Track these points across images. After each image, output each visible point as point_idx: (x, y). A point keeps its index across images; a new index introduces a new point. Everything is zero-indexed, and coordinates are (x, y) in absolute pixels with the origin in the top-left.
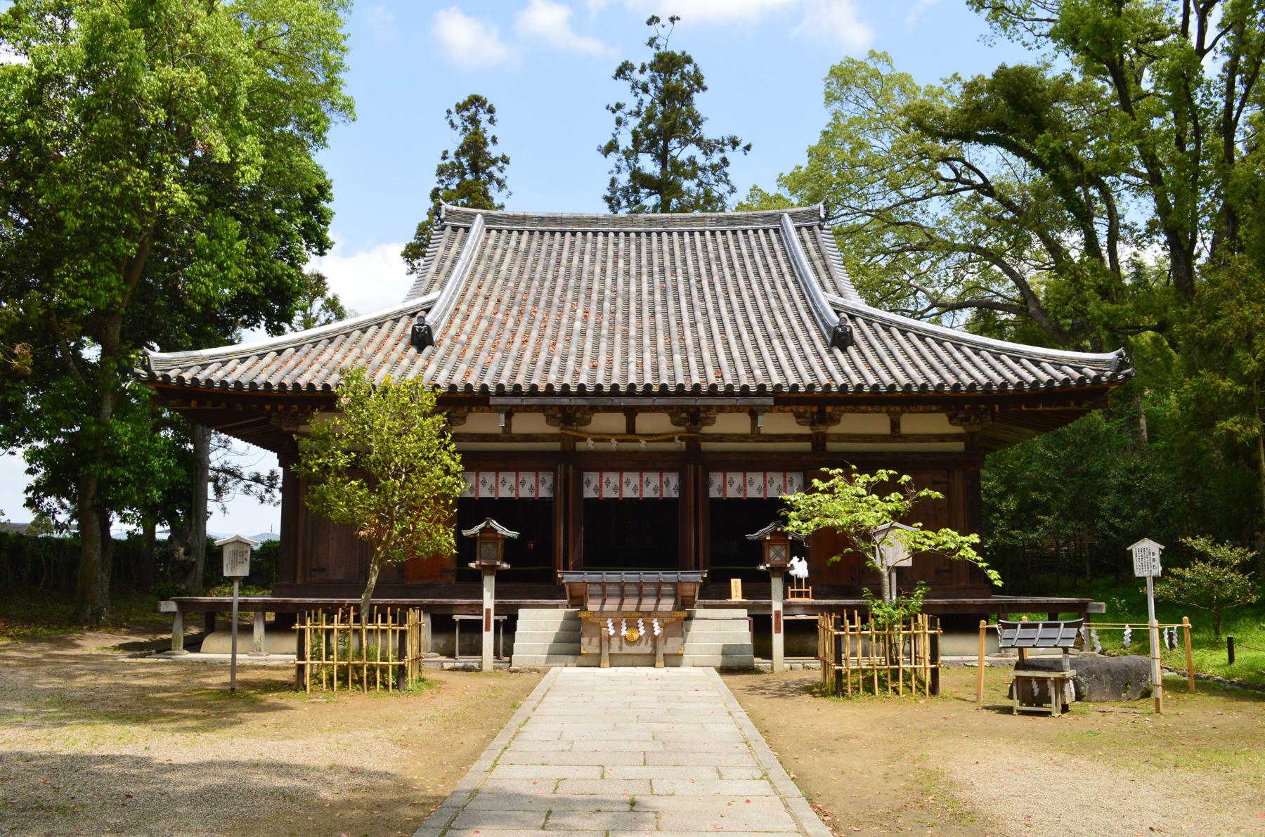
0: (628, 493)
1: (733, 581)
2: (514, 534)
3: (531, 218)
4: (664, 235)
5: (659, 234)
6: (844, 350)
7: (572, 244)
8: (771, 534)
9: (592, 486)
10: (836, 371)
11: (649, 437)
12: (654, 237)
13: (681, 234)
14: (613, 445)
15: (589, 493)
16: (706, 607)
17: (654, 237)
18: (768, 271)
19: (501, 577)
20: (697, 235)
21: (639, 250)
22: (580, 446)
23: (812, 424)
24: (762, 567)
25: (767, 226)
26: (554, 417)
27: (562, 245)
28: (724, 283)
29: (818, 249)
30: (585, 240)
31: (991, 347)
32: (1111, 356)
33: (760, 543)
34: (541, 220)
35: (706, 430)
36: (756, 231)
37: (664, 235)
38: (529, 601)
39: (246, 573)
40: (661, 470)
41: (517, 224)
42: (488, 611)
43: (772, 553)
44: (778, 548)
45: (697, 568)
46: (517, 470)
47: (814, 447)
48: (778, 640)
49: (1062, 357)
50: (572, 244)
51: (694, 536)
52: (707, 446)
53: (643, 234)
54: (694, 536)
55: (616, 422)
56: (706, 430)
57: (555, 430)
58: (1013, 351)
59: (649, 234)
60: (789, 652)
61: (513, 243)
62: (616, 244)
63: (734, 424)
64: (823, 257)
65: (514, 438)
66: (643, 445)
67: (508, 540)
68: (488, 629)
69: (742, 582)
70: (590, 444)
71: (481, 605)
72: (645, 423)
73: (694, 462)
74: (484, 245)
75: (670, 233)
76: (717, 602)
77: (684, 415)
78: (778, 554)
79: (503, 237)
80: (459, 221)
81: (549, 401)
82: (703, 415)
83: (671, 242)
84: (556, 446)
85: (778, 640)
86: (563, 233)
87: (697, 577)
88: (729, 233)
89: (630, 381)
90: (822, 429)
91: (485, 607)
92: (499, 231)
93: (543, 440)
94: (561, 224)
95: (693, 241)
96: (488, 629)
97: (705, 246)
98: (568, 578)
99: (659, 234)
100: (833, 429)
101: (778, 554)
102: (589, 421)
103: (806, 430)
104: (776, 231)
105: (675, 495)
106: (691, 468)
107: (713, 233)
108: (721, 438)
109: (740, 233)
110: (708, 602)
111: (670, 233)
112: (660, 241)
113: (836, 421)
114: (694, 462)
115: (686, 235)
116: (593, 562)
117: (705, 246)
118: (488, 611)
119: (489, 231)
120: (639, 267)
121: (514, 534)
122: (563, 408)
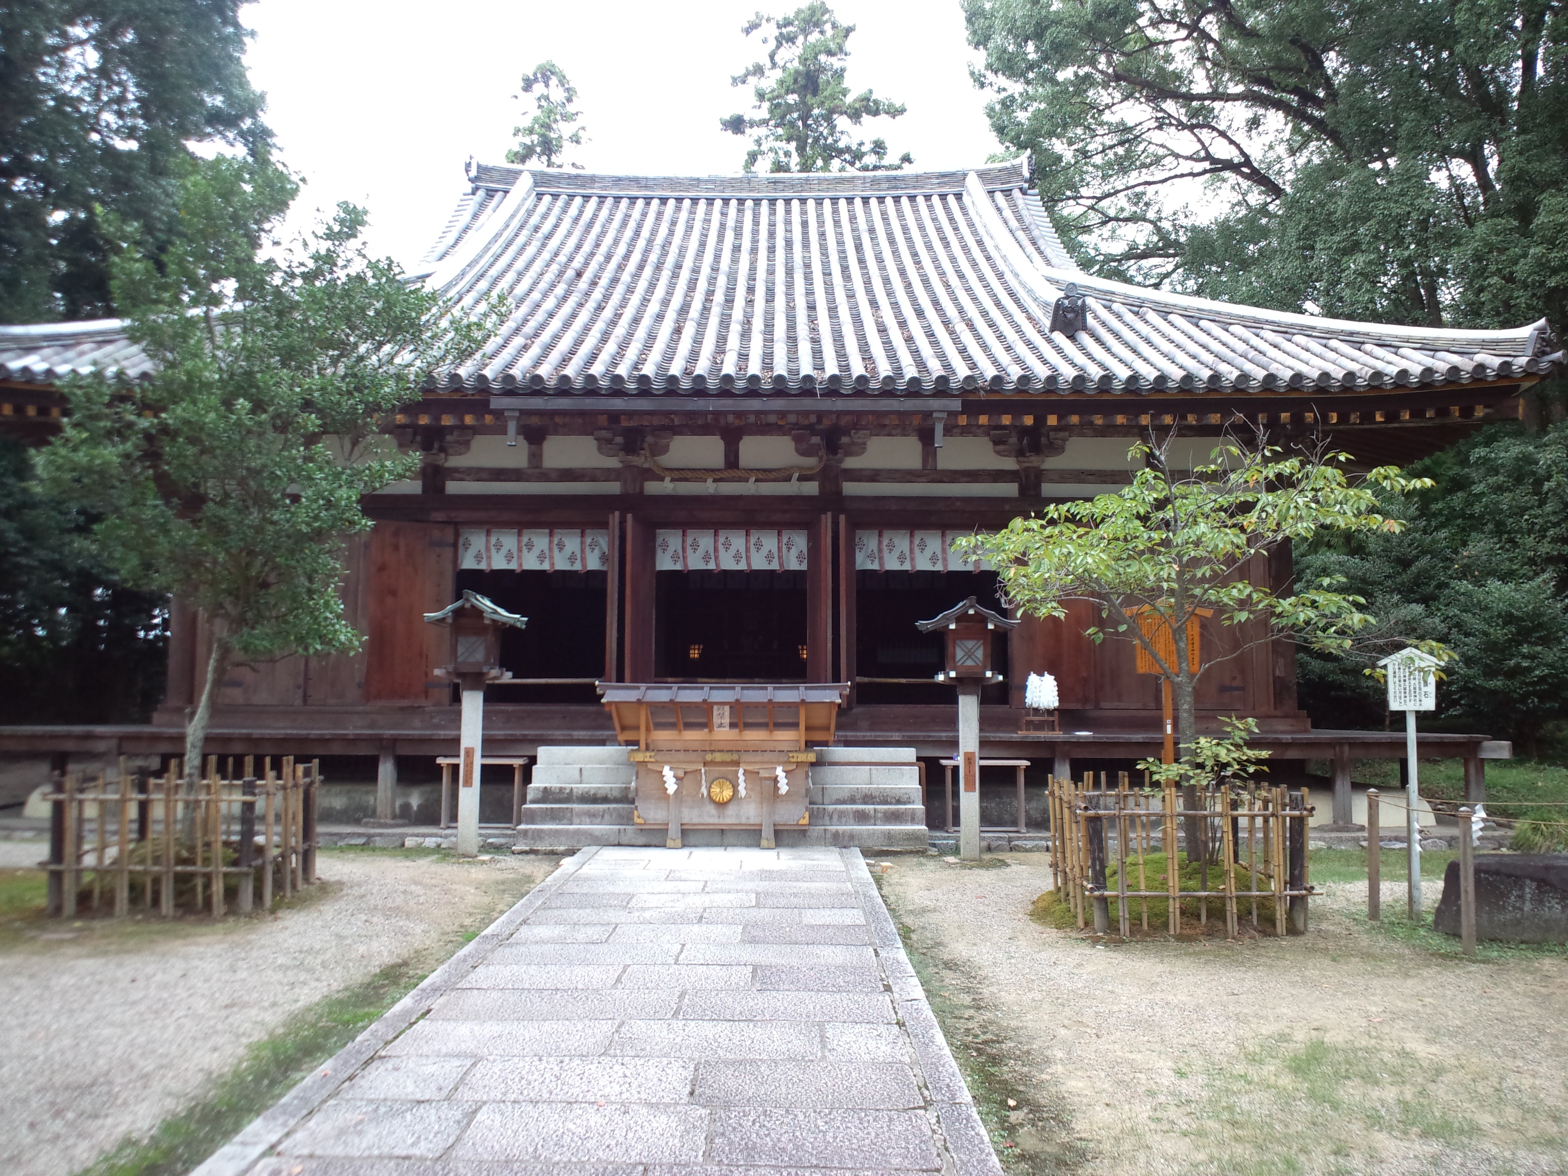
0: (728, 563)
1: (962, 699)
2: (518, 619)
3: (603, 178)
4: (795, 204)
5: (788, 201)
6: (1072, 337)
7: (660, 215)
8: (958, 620)
9: (670, 551)
10: (1063, 361)
11: (765, 474)
12: (780, 205)
13: (819, 202)
14: (709, 487)
15: (665, 563)
16: (848, 743)
17: (780, 205)
18: (947, 245)
19: (495, 695)
20: (842, 203)
21: (756, 223)
22: (652, 488)
23: (1020, 453)
24: (941, 677)
25: (945, 190)
26: (609, 441)
27: (644, 215)
28: (880, 259)
29: (1020, 219)
30: (678, 209)
31: (1313, 328)
32: (1526, 332)
33: (939, 638)
34: (618, 181)
35: (851, 463)
36: (928, 198)
37: (795, 204)
38: (558, 734)
39: (1429, 704)
40: (779, 526)
41: (583, 186)
42: (469, 752)
43: (959, 654)
44: (970, 644)
45: (836, 678)
46: (552, 526)
47: (1022, 490)
48: (970, 802)
49: (1437, 339)
50: (660, 215)
51: (830, 625)
52: (850, 488)
53: (765, 203)
54: (830, 625)
55: (707, 450)
56: (851, 463)
57: (613, 463)
58: (1351, 334)
59: (772, 202)
60: (986, 819)
61: (573, 211)
62: (724, 214)
63: (896, 452)
64: (1026, 229)
65: (545, 476)
66: (750, 488)
67: (505, 632)
68: (468, 783)
69: (1385, 703)
70: (666, 487)
71: (457, 741)
72: (756, 450)
73: (831, 511)
74: (530, 213)
75: (803, 201)
76: (869, 735)
77: (816, 440)
78: (969, 654)
79: (560, 203)
80: (497, 182)
81: (589, 403)
82: (845, 440)
83: (804, 212)
84: (613, 488)
85: (970, 802)
86: (648, 200)
87: (831, 695)
88: (889, 201)
89: (725, 371)
90: (1034, 461)
91: (465, 743)
92: (555, 197)
93: (593, 479)
94: (646, 187)
95: (836, 212)
96: (468, 783)
97: (853, 219)
98: (613, 695)
99: (788, 201)
100: (1051, 463)
101: (969, 654)
102: (665, 449)
103: (1010, 464)
104: (959, 197)
105: (804, 567)
106: (827, 519)
107: (866, 200)
108: (874, 476)
109: (905, 201)
110: (850, 735)
111: (803, 201)
112: (788, 212)
113: (1056, 449)
114: (831, 511)
115: (827, 203)
116: (674, 667)
117: (853, 219)
118: (469, 752)
119: (540, 196)
120: (755, 241)
121: (518, 619)
122: (614, 416)
